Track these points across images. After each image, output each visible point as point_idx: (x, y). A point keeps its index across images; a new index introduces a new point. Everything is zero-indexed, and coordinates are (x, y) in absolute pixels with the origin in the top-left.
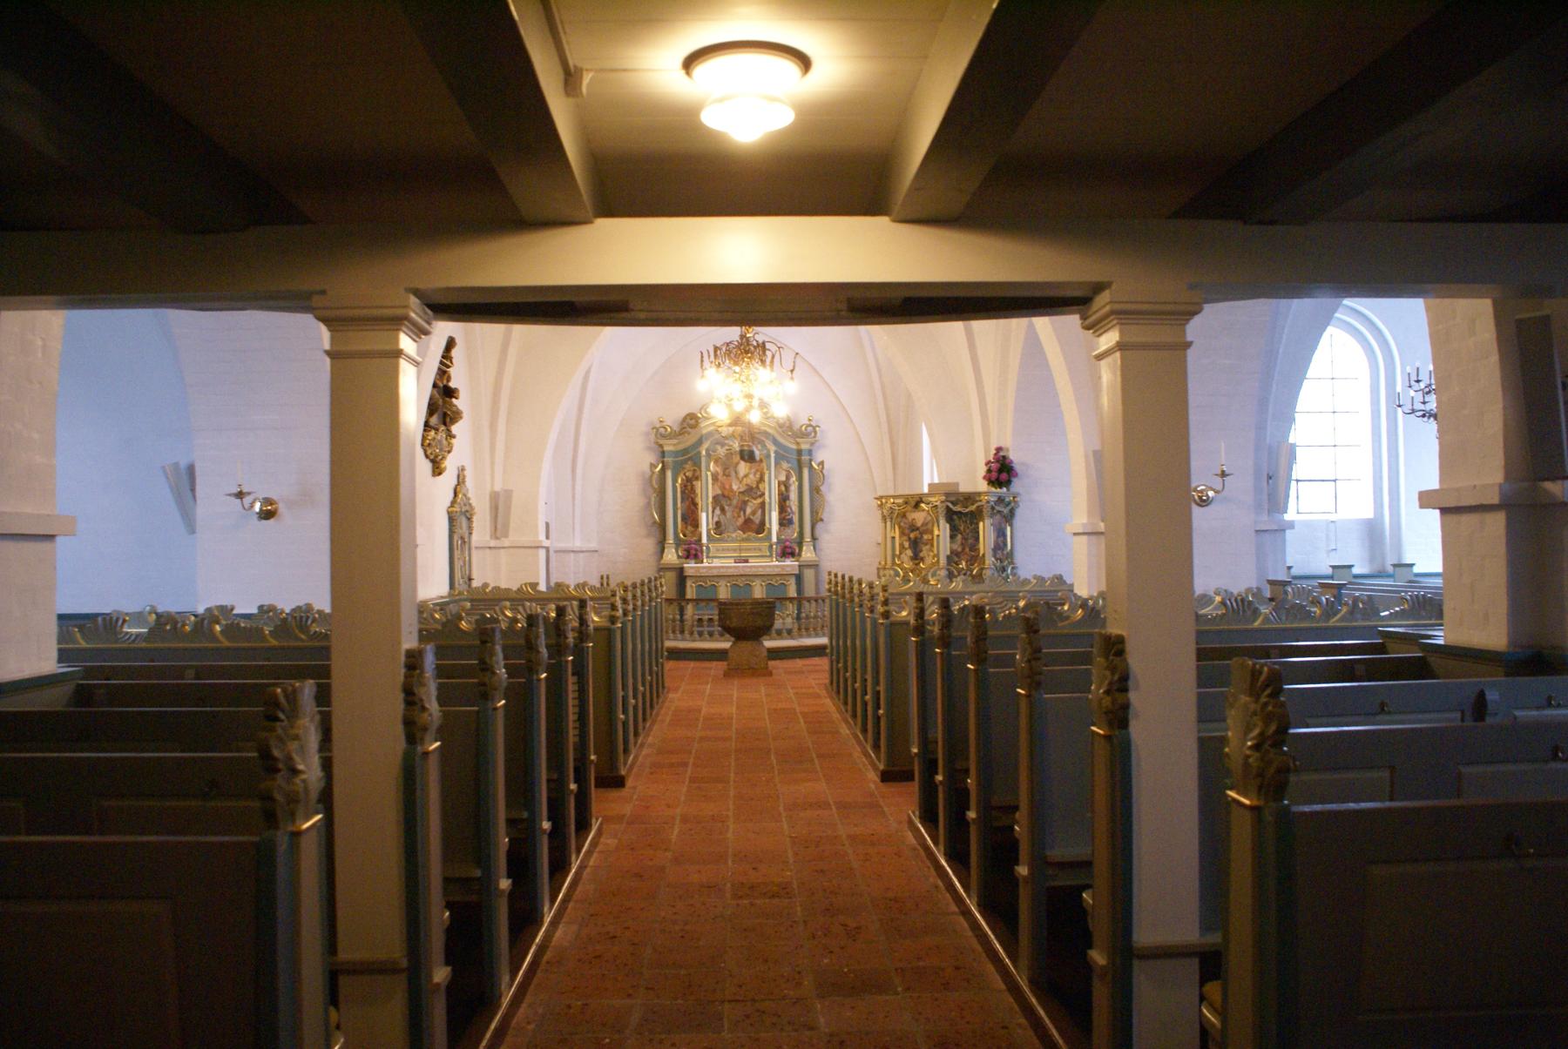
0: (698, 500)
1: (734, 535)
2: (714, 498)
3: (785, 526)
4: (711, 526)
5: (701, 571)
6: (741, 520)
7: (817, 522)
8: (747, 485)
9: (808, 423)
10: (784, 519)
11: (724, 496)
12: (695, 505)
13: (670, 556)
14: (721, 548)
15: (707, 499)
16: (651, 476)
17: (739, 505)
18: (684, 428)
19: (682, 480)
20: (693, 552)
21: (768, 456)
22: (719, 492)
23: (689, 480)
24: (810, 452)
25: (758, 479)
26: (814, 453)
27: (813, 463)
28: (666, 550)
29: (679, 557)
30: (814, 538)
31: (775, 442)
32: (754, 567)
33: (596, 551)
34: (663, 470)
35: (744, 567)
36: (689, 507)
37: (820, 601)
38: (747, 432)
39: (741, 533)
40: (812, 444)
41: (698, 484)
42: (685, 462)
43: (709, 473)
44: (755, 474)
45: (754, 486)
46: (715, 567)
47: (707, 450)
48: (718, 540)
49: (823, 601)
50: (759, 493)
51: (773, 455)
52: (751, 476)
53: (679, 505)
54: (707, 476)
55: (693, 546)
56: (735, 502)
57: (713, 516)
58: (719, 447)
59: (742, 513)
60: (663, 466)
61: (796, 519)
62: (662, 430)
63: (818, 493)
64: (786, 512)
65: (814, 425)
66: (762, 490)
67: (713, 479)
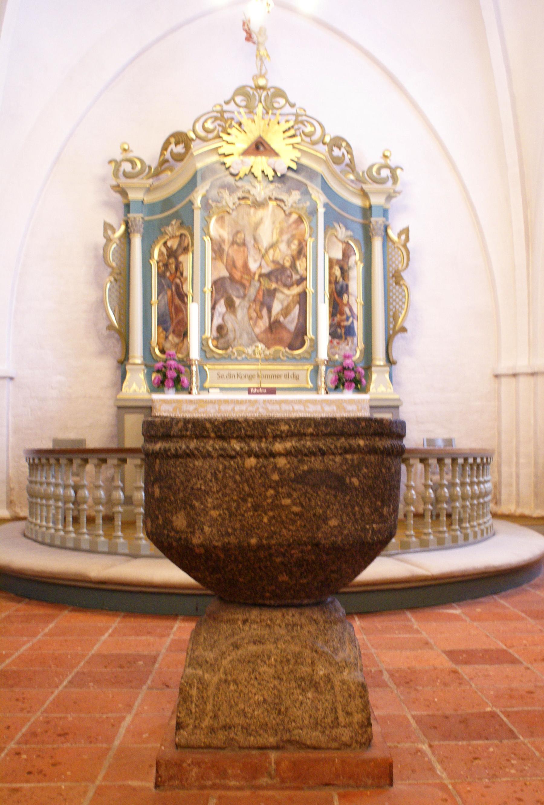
0: (187, 288)
1: (250, 350)
2: (215, 283)
3: (340, 337)
4: (208, 334)
5: (185, 407)
6: (263, 324)
7: (395, 333)
8: (273, 262)
9: (382, 161)
10: (339, 325)
11: (232, 278)
12: (182, 297)
13: (134, 386)
14: (225, 373)
15: (203, 284)
16: (105, 248)
17: (260, 297)
19: (161, 253)
20: (171, 374)
21: (313, 212)
22: (225, 273)
23: (172, 254)
24: (385, 212)
25: (295, 253)
26: (390, 214)
27: (390, 232)
28: (128, 375)
30: (390, 361)
31: (326, 188)
32: (287, 402)
33: (11, 379)
34: (127, 236)
35: (265, 401)
37: (433, 462)
40: (389, 197)
41: (186, 260)
42: (166, 222)
43: (207, 239)
44: (289, 244)
45: (288, 264)
46: (212, 402)
47: (205, 199)
48: (222, 357)
49: (440, 461)
50: (295, 277)
51: (321, 211)
52: (283, 246)
53: (154, 298)
54: (203, 242)
56: (252, 292)
58: (226, 194)
59: (265, 312)
61: (359, 327)
62: (127, 167)
63: (397, 283)
64: (342, 313)
67: (213, 250)
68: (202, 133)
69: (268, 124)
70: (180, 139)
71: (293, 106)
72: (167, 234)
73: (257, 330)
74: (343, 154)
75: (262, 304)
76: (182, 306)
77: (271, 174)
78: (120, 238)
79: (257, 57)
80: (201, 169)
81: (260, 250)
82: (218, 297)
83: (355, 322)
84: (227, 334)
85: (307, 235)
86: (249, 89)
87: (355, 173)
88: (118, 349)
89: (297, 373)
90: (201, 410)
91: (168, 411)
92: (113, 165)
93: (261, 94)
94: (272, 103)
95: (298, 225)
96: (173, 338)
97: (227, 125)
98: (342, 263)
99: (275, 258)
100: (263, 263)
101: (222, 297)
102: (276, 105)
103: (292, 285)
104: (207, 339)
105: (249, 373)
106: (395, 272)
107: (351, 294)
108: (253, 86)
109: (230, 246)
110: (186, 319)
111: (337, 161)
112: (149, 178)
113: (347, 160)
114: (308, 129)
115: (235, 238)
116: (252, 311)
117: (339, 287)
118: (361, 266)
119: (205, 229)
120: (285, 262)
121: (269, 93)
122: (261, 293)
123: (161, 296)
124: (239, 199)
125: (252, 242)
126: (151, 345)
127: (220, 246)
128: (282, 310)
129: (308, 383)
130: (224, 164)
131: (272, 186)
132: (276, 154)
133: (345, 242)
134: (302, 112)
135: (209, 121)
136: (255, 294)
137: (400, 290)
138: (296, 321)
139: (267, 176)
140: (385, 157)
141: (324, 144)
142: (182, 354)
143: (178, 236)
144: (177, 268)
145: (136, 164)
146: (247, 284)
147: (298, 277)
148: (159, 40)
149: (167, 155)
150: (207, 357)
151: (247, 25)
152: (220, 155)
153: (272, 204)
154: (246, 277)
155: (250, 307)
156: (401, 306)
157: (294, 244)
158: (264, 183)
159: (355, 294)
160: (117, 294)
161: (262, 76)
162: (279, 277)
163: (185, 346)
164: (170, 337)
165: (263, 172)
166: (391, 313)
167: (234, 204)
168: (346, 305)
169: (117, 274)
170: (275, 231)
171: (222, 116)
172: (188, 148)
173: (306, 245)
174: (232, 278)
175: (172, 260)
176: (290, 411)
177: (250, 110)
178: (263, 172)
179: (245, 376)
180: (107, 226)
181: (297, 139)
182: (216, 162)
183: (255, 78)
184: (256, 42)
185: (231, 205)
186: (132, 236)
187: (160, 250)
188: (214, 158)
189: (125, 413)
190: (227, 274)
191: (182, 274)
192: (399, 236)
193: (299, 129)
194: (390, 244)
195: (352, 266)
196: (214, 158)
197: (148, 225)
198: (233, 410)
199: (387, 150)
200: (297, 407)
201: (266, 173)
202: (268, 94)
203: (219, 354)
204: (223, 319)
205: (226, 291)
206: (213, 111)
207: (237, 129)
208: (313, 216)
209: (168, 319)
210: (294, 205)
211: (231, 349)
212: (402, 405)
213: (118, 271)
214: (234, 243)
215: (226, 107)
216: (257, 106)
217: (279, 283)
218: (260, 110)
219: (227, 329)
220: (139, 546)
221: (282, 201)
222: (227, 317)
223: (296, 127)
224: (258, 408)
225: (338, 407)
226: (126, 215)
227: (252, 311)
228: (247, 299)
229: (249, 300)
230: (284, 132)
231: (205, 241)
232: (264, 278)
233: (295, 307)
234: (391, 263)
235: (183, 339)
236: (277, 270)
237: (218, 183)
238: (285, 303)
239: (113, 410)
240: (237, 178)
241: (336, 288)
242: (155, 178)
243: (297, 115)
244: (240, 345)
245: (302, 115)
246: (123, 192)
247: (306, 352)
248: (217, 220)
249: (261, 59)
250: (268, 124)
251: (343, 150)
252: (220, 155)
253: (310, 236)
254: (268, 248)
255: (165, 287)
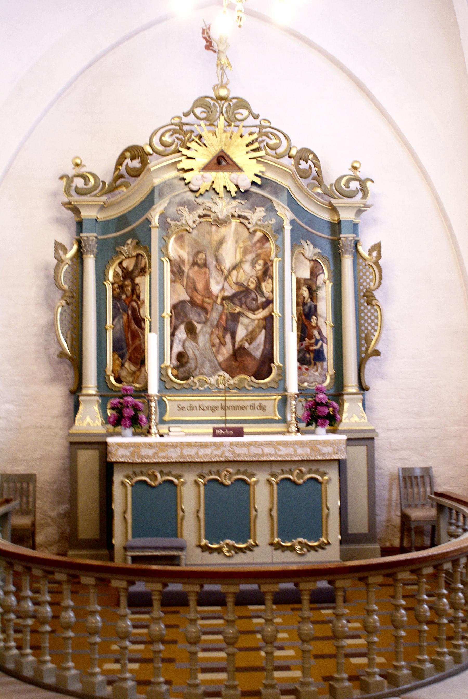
0: (145, 312)
1: (212, 380)
2: (174, 307)
4: (167, 362)
5: (144, 452)
6: (227, 351)
7: (368, 356)
8: (237, 283)
9: (351, 173)
10: (308, 350)
11: (192, 302)
12: (139, 321)
13: (88, 420)
14: (186, 405)
15: (162, 309)
17: (223, 322)
18: (122, 176)
19: (116, 274)
20: (129, 412)
21: (280, 229)
24: (355, 227)
25: (260, 273)
27: (360, 248)
28: (81, 408)
29: (107, 420)
30: (363, 388)
35: (231, 444)
36: (128, 326)
38: (228, 313)
39: (227, 375)
40: (359, 212)
42: (121, 241)
43: (165, 260)
44: (253, 264)
45: (252, 286)
46: (173, 446)
47: (163, 216)
48: (184, 388)
50: (261, 300)
51: (288, 228)
52: (247, 267)
55: (129, 399)
56: (214, 316)
57: (172, 342)
58: (185, 211)
59: (228, 338)
60: (80, 247)
62: (79, 182)
64: (311, 337)
65: (363, 178)
66: (267, 294)
67: (172, 272)
68: (160, 148)
69: (231, 137)
70: (136, 153)
71: (256, 117)
72: (122, 254)
73: (221, 358)
74: (310, 166)
75: (226, 329)
76: (139, 331)
77: (233, 189)
78: (72, 259)
79: (217, 66)
80: (159, 185)
81: (222, 271)
82: (178, 322)
83: (325, 345)
84: (187, 362)
85: (273, 255)
86: (209, 100)
87: (323, 187)
88: (70, 375)
89: (264, 403)
90: (161, 454)
91: (125, 456)
92: (65, 180)
93: (223, 105)
94: (234, 114)
95: (263, 244)
96: (129, 366)
97: (186, 139)
98: (310, 282)
99: (239, 280)
100: (226, 285)
101: (182, 322)
102: (238, 116)
103: (258, 309)
104: (167, 368)
105: (212, 404)
106: (367, 291)
107: (320, 316)
108: (214, 97)
109: (190, 268)
110: (143, 345)
111: (304, 174)
112: (102, 195)
113: (314, 173)
114: (273, 142)
115: (196, 259)
116: (214, 336)
117: (307, 310)
118: (330, 285)
119: (163, 250)
120: (250, 283)
121: (231, 103)
122: (224, 317)
123: (116, 320)
124: (200, 217)
125: (214, 263)
126: (105, 372)
127: (180, 268)
128: (246, 336)
129: (276, 415)
130: (184, 179)
131: (235, 203)
132: (240, 169)
133: (313, 260)
134: (268, 124)
135: (168, 134)
136: (218, 318)
137: (372, 311)
138: (262, 347)
139: (229, 192)
140: (355, 168)
141: (290, 157)
142: (139, 383)
143: (134, 256)
144: (133, 290)
145: (89, 181)
146: (209, 308)
147: (264, 300)
148: (112, 48)
149: (123, 169)
150: (166, 388)
151: (207, 33)
152: (179, 170)
153: (234, 222)
154: (207, 300)
155: (212, 333)
156: (373, 328)
157: (260, 265)
158: (227, 199)
159: (325, 315)
160: (68, 318)
161: (224, 86)
162: (243, 300)
163: (142, 375)
164: (127, 365)
165: (225, 187)
166: (363, 335)
167: (194, 222)
168: (314, 328)
169: (70, 297)
170: (238, 250)
171: (181, 129)
172: (144, 163)
173: (272, 265)
174: (192, 302)
175: (127, 282)
176: (259, 455)
177: (211, 122)
178: (225, 187)
179: (207, 408)
180: (59, 247)
181: (262, 153)
182: (175, 178)
183: (216, 88)
184: (217, 51)
185: (191, 224)
186: (84, 256)
187: (115, 271)
188: (173, 173)
189: (80, 449)
190: (188, 298)
191: (138, 297)
192: (370, 253)
193: (263, 141)
194: (361, 260)
195: (320, 286)
196: (173, 173)
197: (102, 244)
198: (197, 454)
199: (356, 161)
200: (267, 450)
201: (228, 189)
202: (229, 104)
203: (179, 384)
204: (184, 347)
205: (186, 316)
206: (172, 124)
207: (196, 142)
208: (279, 234)
209: (124, 344)
210: (259, 222)
211: (192, 378)
212: (377, 436)
213: (70, 294)
214: (194, 263)
215: (185, 120)
216: (219, 117)
217: (244, 306)
218: (221, 122)
219: (188, 357)
220: (93, 684)
221: (245, 218)
222: (187, 344)
223: (260, 139)
224: (224, 452)
225: (312, 450)
226: (78, 234)
227: (214, 336)
228: (209, 324)
229: (212, 325)
230: (247, 146)
231: (163, 261)
232: (227, 301)
233: (260, 332)
234: (362, 281)
235: (140, 368)
236: (242, 292)
237: (177, 200)
238: (250, 328)
239: (64, 443)
240: (197, 194)
241: (304, 310)
242: (109, 195)
243: (261, 127)
244: (202, 374)
245: (266, 127)
246: (76, 210)
247: (273, 380)
248: (176, 240)
249: (222, 68)
250: (231, 137)
251: (310, 162)
252: (179, 170)
253: (276, 256)
254: (231, 269)
255: (121, 310)
